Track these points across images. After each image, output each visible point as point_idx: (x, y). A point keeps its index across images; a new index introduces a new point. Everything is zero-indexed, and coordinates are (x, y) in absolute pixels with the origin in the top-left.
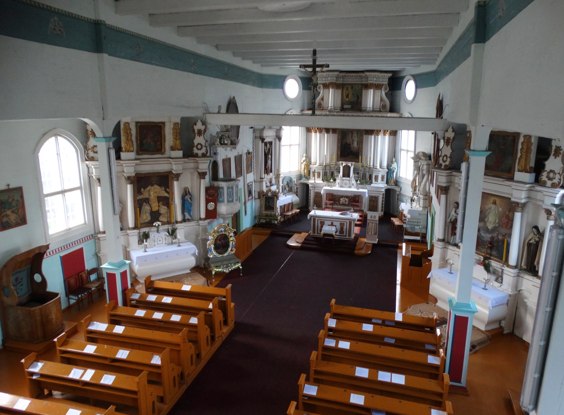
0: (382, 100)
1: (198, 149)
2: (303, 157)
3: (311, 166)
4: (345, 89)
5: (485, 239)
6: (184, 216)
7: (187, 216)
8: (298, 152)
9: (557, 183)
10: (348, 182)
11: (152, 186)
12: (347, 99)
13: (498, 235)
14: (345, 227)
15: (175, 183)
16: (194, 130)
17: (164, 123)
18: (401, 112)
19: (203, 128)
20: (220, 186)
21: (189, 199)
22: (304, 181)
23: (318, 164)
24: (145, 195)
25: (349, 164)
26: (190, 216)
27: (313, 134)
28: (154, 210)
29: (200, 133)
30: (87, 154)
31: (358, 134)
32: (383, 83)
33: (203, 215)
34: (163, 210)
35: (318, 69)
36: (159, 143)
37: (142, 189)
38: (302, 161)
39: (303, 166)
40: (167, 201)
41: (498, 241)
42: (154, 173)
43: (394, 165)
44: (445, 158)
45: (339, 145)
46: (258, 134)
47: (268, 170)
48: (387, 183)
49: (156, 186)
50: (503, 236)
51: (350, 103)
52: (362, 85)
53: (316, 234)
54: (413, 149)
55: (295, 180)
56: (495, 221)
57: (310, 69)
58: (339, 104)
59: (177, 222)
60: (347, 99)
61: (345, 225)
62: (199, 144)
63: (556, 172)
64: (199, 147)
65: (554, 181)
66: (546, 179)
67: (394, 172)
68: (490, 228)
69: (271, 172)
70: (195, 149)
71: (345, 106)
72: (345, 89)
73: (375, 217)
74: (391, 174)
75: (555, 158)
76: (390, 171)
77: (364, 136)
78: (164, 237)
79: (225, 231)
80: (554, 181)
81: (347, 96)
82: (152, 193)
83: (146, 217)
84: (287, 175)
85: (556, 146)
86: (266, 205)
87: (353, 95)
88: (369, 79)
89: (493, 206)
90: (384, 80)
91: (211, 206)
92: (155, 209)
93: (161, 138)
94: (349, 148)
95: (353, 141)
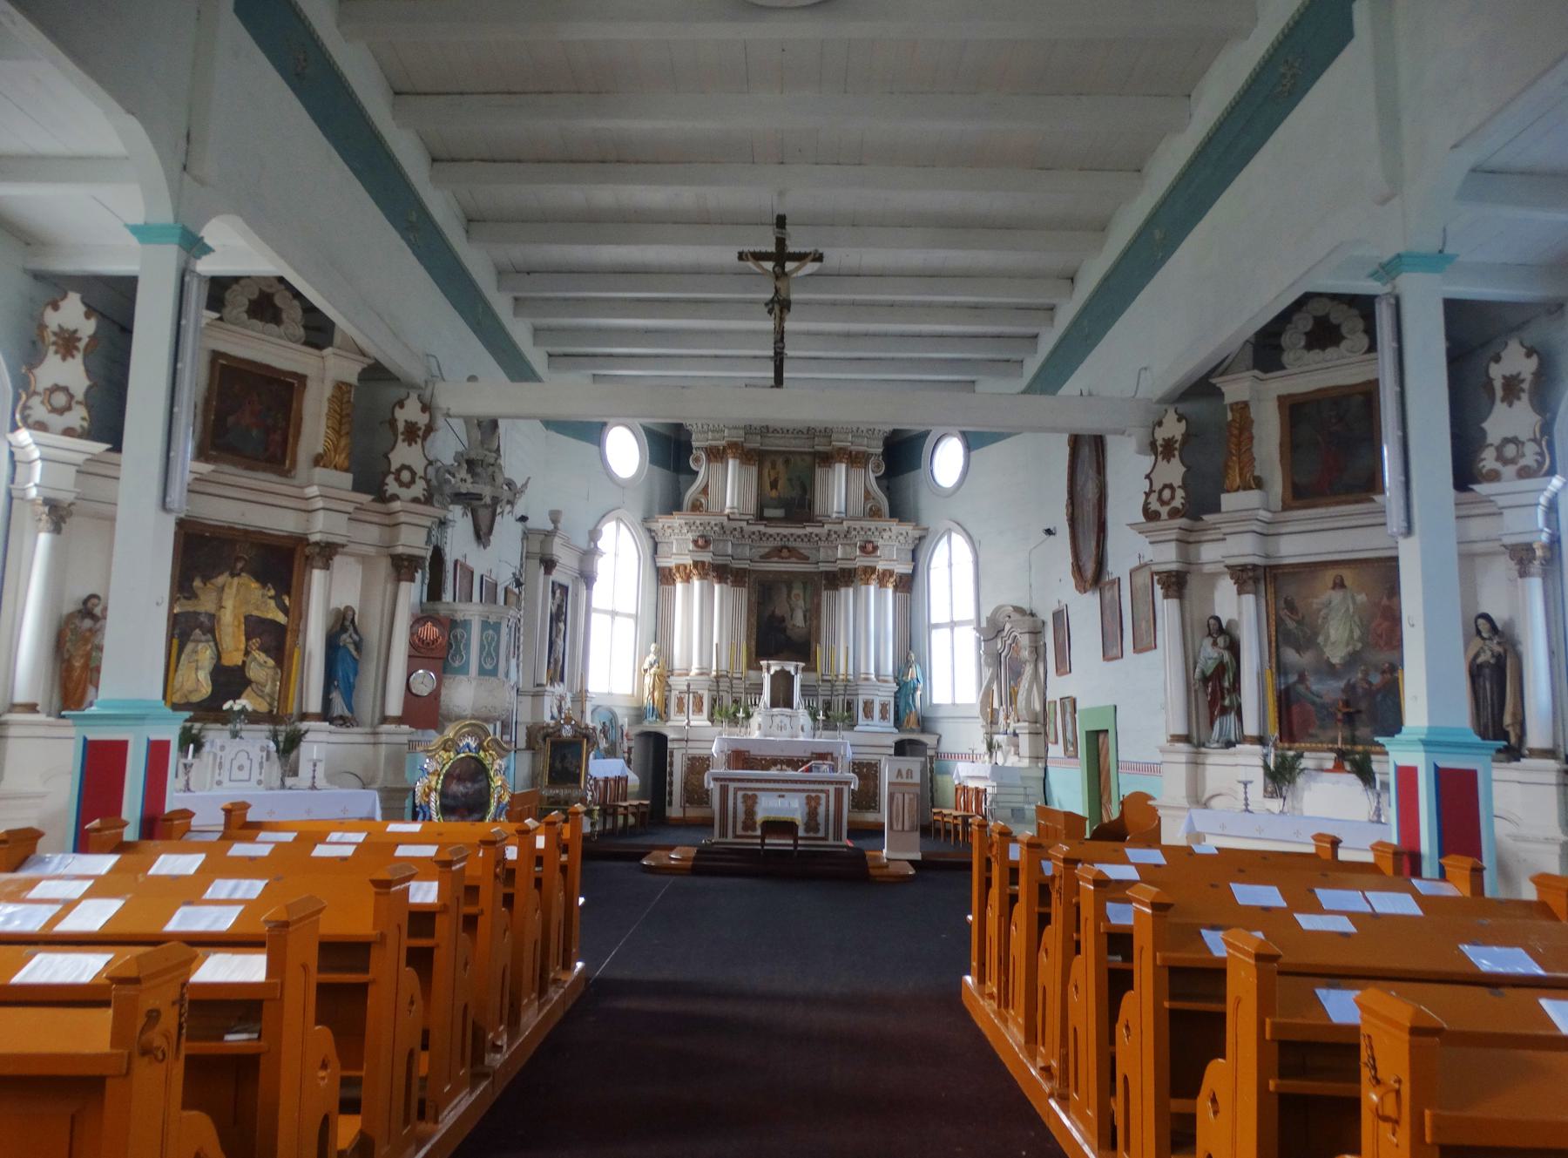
0: (868, 495)
1: (401, 484)
2: (648, 653)
3: (673, 680)
4: (768, 465)
5: (1327, 699)
6: (327, 702)
7: (339, 707)
8: (636, 634)
9: (1535, 465)
10: (786, 721)
11: (233, 575)
12: (774, 494)
13: (1366, 673)
14: (822, 810)
15: (317, 576)
16: (393, 422)
17: (302, 379)
18: (924, 524)
19: (422, 420)
20: (459, 617)
21: (352, 648)
22: (651, 725)
23: (694, 671)
24: (206, 604)
25: (790, 667)
26: (350, 708)
27: (679, 586)
28: (226, 662)
29: (412, 433)
30: (25, 407)
31: (805, 588)
32: (871, 450)
33: (395, 707)
34: (261, 668)
35: (789, 266)
36: (277, 437)
37: (197, 583)
38: (646, 666)
39: (648, 680)
40: (277, 640)
41: (1370, 693)
42: (246, 532)
43: (914, 672)
44: (1167, 494)
45: (754, 620)
46: (535, 548)
47: (557, 675)
48: (898, 723)
49: (245, 577)
50: (1383, 672)
51: (781, 503)
52: (815, 455)
53: (730, 839)
54: (971, 615)
55: (624, 721)
56: (1351, 637)
57: (769, 265)
58: (751, 507)
59: (304, 717)
60: (774, 494)
61: (823, 801)
62: (404, 467)
63: (1522, 438)
64: (406, 476)
65: (1523, 462)
66: (1498, 466)
67: (915, 689)
68: (1335, 660)
69: (562, 680)
70: (390, 479)
71: (768, 513)
72: (768, 465)
73: (910, 773)
74: (907, 696)
75: (1510, 405)
76: (904, 690)
77: (824, 594)
78: (257, 754)
79: (480, 747)
80: (1523, 462)
81: (774, 485)
82: (229, 603)
83: (197, 681)
84: (605, 703)
85: (1504, 377)
86: (552, 767)
87: (790, 480)
88: (834, 436)
89: (1336, 596)
90: (874, 443)
91: (424, 682)
92: (233, 658)
93: (287, 419)
94: (781, 626)
95: (792, 610)
